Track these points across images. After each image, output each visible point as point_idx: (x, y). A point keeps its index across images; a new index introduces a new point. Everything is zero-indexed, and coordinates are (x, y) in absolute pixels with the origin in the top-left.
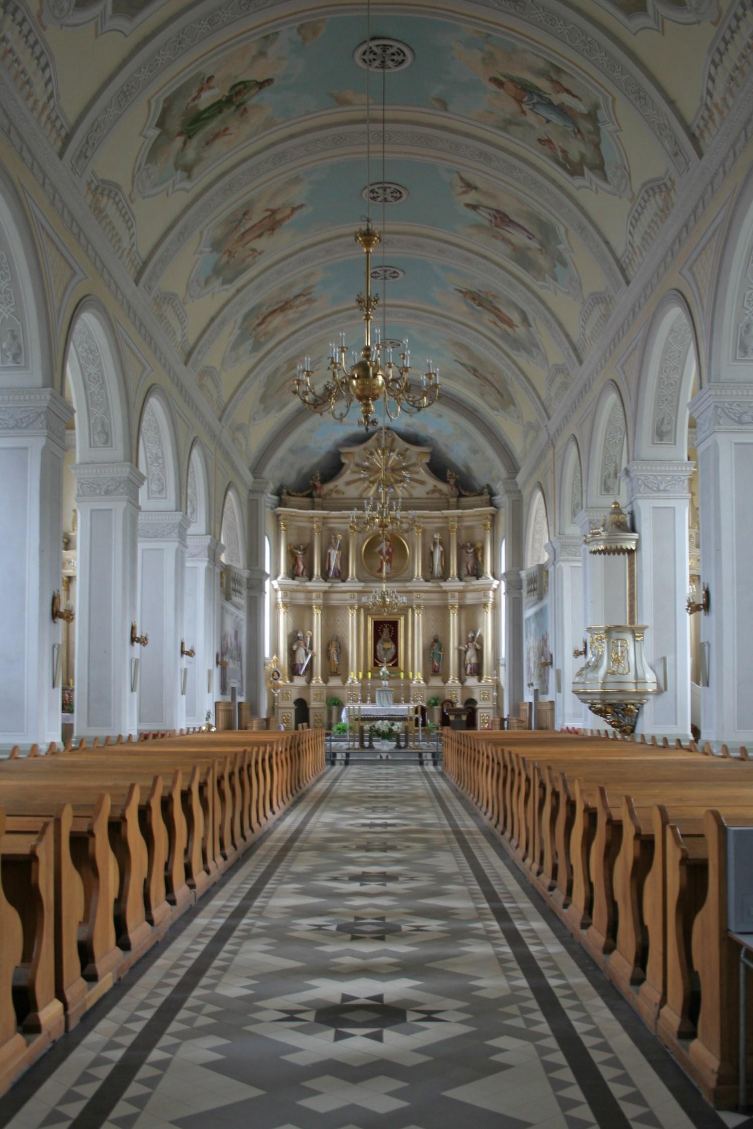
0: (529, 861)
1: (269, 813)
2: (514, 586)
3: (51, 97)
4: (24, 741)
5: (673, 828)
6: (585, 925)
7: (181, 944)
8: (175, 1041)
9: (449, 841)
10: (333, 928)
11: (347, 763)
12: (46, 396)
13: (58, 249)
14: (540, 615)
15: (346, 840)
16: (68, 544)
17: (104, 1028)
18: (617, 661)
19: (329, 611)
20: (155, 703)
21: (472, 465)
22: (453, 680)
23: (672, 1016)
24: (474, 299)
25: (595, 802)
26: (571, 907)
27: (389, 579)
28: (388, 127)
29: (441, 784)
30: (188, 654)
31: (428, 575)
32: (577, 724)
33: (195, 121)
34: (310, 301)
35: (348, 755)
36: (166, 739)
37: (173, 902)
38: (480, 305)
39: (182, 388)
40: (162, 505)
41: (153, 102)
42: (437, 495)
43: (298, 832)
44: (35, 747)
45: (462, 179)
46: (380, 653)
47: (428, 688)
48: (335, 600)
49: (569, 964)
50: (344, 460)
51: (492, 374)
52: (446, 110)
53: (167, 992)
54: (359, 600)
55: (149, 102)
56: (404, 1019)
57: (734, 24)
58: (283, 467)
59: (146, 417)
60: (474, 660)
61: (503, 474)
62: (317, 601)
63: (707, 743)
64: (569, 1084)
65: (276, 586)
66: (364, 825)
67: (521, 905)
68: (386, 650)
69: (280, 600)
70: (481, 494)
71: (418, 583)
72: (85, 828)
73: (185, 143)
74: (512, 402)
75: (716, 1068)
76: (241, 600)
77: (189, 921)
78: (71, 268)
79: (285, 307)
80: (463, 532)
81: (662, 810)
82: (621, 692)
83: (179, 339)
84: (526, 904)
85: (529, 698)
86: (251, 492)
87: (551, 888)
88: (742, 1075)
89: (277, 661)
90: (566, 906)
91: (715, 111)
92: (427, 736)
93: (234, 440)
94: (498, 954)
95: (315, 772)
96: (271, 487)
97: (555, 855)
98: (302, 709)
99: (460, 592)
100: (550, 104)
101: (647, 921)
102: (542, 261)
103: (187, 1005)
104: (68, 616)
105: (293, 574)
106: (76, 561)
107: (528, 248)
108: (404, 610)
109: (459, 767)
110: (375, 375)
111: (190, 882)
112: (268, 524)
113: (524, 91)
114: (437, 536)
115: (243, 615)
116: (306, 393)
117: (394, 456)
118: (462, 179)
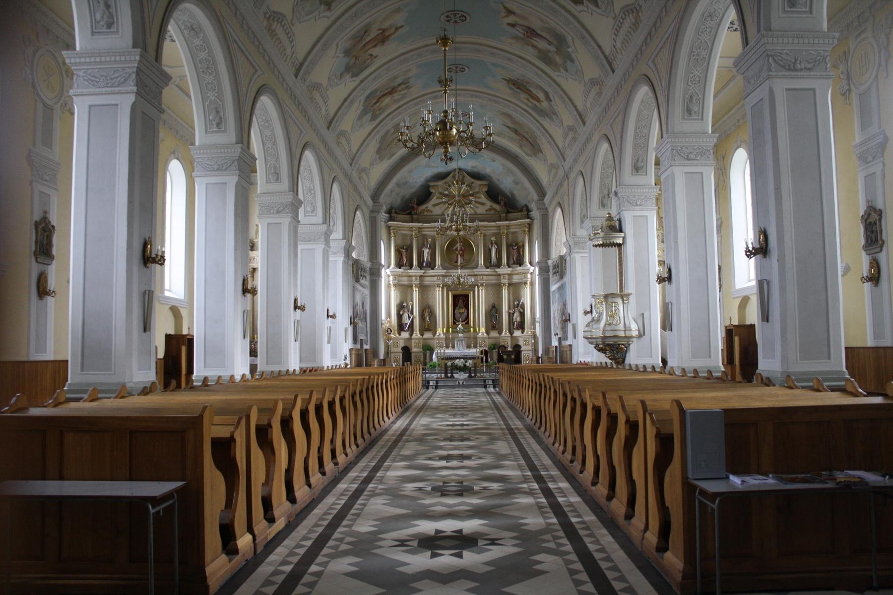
0: (557, 445)
1: (386, 418)
2: (544, 271)
4: (225, 374)
5: (651, 414)
6: (594, 484)
7: (329, 500)
8: (326, 559)
9: (504, 434)
10: (429, 489)
11: (436, 387)
12: (238, 149)
13: (245, 55)
14: (562, 288)
15: (436, 435)
16: (253, 247)
17: (280, 552)
18: (612, 316)
19: (423, 288)
20: (310, 349)
21: (515, 192)
22: (505, 333)
23: (652, 538)
24: (514, 84)
25: (599, 403)
26: (585, 472)
27: (462, 267)
29: (497, 399)
30: (331, 317)
31: (488, 264)
32: (587, 359)
34: (408, 87)
35: (437, 382)
36: (318, 372)
37: (324, 474)
38: (518, 88)
39: (326, 145)
40: (314, 220)
42: (493, 212)
43: (405, 430)
44: (232, 377)
45: (505, 8)
46: (457, 315)
47: (489, 338)
48: (428, 281)
49: (584, 508)
50: (432, 190)
51: (527, 133)
53: (320, 530)
54: (443, 281)
56: (476, 544)
58: (391, 196)
59: (302, 163)
60: (518, 319)
61: (536, 197)
62: (415, 282)
63: (672, 368)
64: (586, 582)
65: (389, 273)
66: (448, 425)
67: (552, 473)
68: (461, 314)
69: (391, 282)
70: (521, 211)
71: (482, 270)
72: (266, 423)
74: (540, 151)
75: (681, 569)
76: (366, 282)
77: (335, 486)
78: (253, 67)
79: (392, 91)
80: (510, 236)
81: (643, 403)
82: (615, 336)
83: (324, 113)
84: (555, 472)
85: (555, 343)
86: (372, 211)
87: (572, 461)
88: (698, 573)
89: (390, 322)
90: (581, 472)
92: (489, 369)
93: (360, 178)
94: (537, 503)
95: (416, 392)
96: (384, 208)
97: (574, 440)
98: (407, 352)
99: (509, 275)
101: (635, 476)
102: (558, 59)
103: (333, 537)
104: (254, 292)
105: (399, 265)
106: (258, 258)
107: (549, 51)
108: (473, 287)
109: (510, 388)
110: (451, 128)
111: (334, 461)
112: (383, 233)
114: (493, 239)
115: (367, 292)
116: (406, 141)
117: (464, 187)
118: (505, 8)
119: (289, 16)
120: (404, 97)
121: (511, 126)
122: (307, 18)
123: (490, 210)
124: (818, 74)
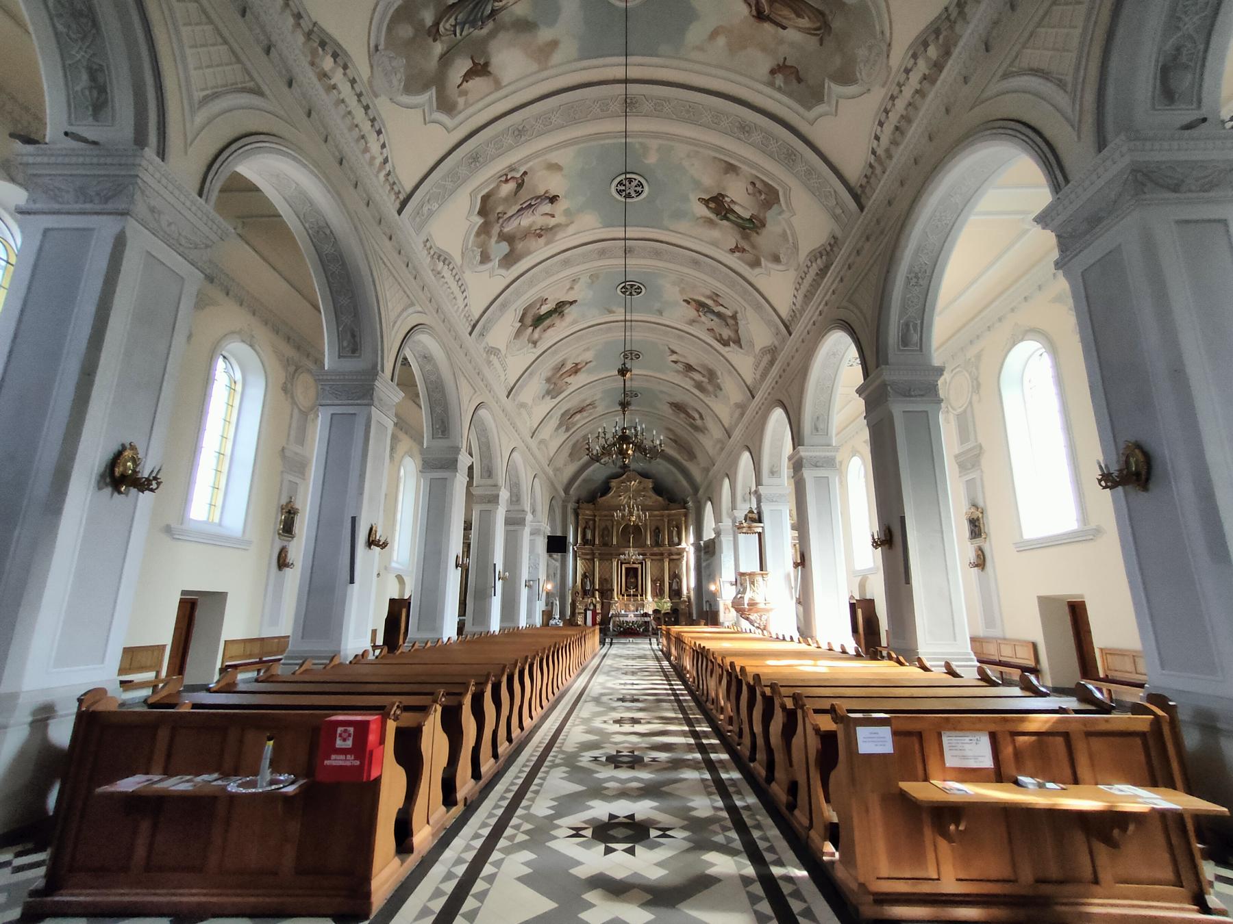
2: (698, 549)
28: (634, 89)
33: (538, 320)
96: (574, 499)
100: (713, 312)
102: (710, 388)
113: (701, 306)
115: (558, 564)
119: (503, 352)
120: (591, 414)
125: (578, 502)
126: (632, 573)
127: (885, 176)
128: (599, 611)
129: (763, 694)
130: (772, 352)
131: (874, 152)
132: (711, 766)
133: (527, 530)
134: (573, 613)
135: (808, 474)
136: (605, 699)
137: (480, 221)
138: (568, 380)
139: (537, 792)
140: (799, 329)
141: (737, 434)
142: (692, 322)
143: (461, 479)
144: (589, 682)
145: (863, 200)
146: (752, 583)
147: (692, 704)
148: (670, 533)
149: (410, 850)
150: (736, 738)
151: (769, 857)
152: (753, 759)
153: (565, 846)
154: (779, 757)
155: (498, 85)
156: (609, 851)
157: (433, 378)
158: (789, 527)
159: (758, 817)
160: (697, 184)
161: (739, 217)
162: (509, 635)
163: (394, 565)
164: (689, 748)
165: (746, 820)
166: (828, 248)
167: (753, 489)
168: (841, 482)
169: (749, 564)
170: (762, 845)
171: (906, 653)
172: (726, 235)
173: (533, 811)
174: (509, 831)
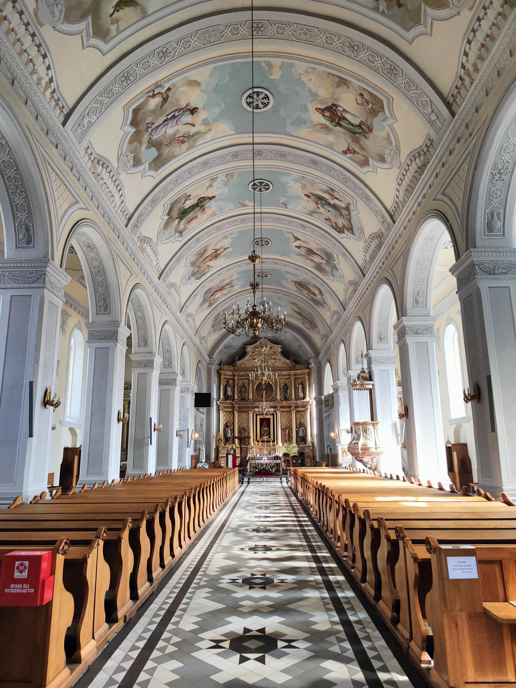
2: (319, 402)
3: (122, 202)
24: (299, 285)
28: (258, 15)
33: (183, 213)
34: (232, 286)
38: (301, 287)
41: (166, 205)
42: (285, 365)
45: (293, 236)
51: (307, 315)
52: (287, 208)
55: (164, 205)
57: (407, 168)
73: (179, 222)
78: (131, 272)
86: (208, 364)
91: (400, 204)
93: (201, 343)
96: (217, 362)
102: (327, 268)
107: (322, 263)
115: (204, 417)
118: (293, 236)
119: (155, 240)
120: (229, 292)
121: (297, 310)
122: (167, 241)
123: (284, 363)
124: (512, 276)
125: (220, 364)
126: (265, 423)
127: (473, 87)
128: (238, 455)
129: (372, 527)
130: (380, 237)
131: (463, 67)
132: (329, 586)
133: (178, 389)
134: (217, 457)
135: (410, 340)
136: (242, 530)
137: (133, 130)
138: (210, 263)
139: (184, 610)
140: (401, 218)
141: (350, 306)
142: (312, 213)
143: (121, 348)
144: (229, 516)
145: (454, 107)
146: (365, 431)
147: (315, 533)
148: (296, 389)
149: (78, 661)
150: (350, 563)
151: (376, 664)
152: (364, 580)
153: (207, 656)
154: (385, 578)
155: (144, 14)
156: (243, 660)
157: (96, 263)
158: (395, 383)
159: (368, 630)
160: (314, 96)
161: (350, 123)
162: (164, 477)
163: (67, 419)
164: (312, 571)
165: (358, 632)
166: (425, 149)
167: (365, 352)
168: (439, 346)
169: (362, 415)
170: (371, 654)
171: (493, 492)
172: (339, 139)
173: (180, 626)
174: (161, 644)
